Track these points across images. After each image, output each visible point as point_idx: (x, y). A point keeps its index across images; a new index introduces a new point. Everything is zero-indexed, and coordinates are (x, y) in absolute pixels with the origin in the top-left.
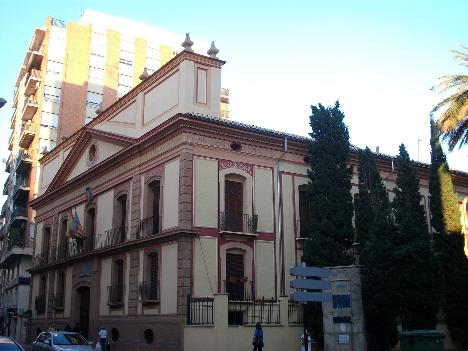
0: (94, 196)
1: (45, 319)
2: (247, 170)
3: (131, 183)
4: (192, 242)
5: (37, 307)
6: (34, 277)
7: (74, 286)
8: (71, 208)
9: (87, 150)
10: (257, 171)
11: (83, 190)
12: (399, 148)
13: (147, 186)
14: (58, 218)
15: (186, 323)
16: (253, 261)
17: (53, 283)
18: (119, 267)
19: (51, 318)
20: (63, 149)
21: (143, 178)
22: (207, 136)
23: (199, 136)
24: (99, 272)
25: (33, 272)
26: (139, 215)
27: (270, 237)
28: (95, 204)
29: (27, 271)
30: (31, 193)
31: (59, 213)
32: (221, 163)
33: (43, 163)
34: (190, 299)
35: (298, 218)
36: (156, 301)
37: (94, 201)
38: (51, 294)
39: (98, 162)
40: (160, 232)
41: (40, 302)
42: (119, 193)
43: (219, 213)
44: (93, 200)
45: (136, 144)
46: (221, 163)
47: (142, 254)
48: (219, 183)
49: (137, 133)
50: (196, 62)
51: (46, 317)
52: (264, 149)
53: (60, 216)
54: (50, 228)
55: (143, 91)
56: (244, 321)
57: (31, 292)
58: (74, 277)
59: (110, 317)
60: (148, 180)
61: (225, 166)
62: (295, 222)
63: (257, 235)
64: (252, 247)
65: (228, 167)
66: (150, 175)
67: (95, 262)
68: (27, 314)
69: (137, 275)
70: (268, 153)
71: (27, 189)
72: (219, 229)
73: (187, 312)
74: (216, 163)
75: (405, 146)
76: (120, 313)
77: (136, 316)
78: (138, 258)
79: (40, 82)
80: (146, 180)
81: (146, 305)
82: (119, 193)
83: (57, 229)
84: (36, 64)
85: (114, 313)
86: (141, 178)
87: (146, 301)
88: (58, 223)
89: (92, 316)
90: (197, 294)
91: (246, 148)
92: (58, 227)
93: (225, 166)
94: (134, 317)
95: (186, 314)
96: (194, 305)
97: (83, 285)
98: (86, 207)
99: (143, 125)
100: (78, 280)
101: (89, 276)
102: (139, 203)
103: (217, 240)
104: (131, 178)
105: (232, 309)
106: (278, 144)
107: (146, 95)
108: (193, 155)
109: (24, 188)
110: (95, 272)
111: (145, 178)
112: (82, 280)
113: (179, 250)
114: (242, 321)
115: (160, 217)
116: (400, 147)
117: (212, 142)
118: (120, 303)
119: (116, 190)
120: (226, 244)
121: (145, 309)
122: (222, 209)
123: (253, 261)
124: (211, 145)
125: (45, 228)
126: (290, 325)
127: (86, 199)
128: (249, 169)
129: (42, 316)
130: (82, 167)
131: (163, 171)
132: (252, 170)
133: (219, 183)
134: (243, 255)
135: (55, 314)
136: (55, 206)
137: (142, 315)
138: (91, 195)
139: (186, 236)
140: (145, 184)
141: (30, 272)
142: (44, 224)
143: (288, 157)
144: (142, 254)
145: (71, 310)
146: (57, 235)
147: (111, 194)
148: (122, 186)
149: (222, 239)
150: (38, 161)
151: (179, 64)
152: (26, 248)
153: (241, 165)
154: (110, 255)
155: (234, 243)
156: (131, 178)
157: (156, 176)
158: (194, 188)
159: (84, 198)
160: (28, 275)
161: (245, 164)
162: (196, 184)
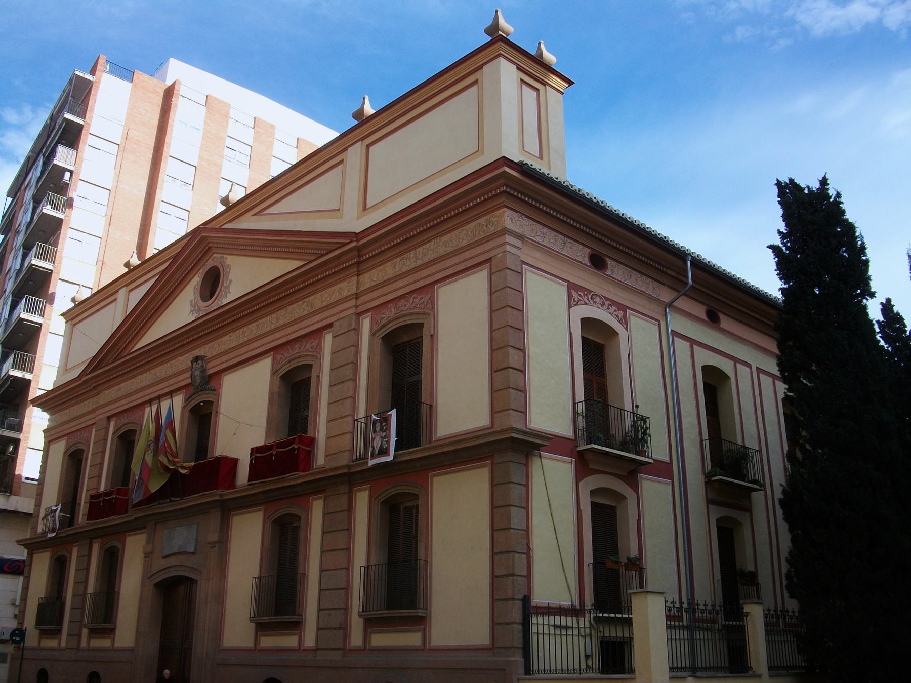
0: (211, 376)
1: (59, 649)
2: (617, 316)
3: (328, 338)
4: (527, 465)
5: (41, 620)
6: (35, 556)
7: (147, 575)
8: (142, 405)
9: (196, 280)
10: (634, 321)
11: (183, 361)
12: (880, 307)
13: (378, 342)
14: (107, 428)
15: (522, 671)
16: (639, 521)
17: (87, 569)
18: (59, 568)
19: (78, 648)
20: (127, 285)
21: (366, 323)
22: (547, 226)
23: (532, 222)
24: (223, 544)
25: (33, 546)
26: (354, 407)
27: (662, 470)
28: (216, 391)
29: (19, 542)
30: (33, 385)
31: (109, 418)
32: (573, 291)
33: (72, 319)
34: (528, 609)
35: (706, 436)
36: (294, 618)
37: (212, 385)
38: (80, 595)
39: (225, 301)
40: (424, 442)
41: (50, 614)
42: (290, 362)
43: (574, 403)
44: (208, 382)
45: (354, 244)
46: (573, 291)
47: (362, 499)
48: (571, 334)
49: (353, 222)
50: (519, 68)
51: (63, 644)
52: (644, 277)
53: (112, 424)
54: (82, 451)
55: (363, 139)
56: (536, 668)
57: (26, 589)
58: (148, 555)
59: (256, 649)
60: (383, 326)
61: (579, 300)
62: (702, 441)
63: (652, 461)
64: (635, 487)
65: (586, 304)
66: (389, 313)
67: (214, 519)
68: (16, 635)
69: (348, 550)
70: (650, 287)
71: (28, 376)
72: (575, 441)
73: (521, 641)
74: (563, 290)
75: (892, 303)
76: (53, 643)
77: (346, 650)
78: (350, 509)
79: (72, 172)
80: (376, 328)
81: (95, 632)
82: (290, 362)
83: (104, 452)
84: (71, 136)
85: (268, 641)
86: (358, 323)
87: (266, 619)
88: (106, 440)
89: (201, 645)
90: (540, 598)
91: (615, 270)
92: (105, 448)
93: (579, 300)
94: (341, 652)
95: (521, 646)
96: (538, 623)
97: (174, 574)
98: (187, 400)
99: (365, 208)
100: (161, 563)
101: (193, 553)
102: (355, 379)
103: (573, 465)
104: (330, 325)
105: (607, 634)
106: (669, 272)
107: (371, 149)
108: (523, 262)
109: (18, 374)
110: (215, 543)
111: (116, 424)
112: (172, 561)
113: (493, 485)
114: (624, 665)
115: (424, 408)
116: (882, 303)
117: (555, 240)
118: (109, 626)
119: (278, 357)
120: (590, 478)
121: (372, 633)
122: (580, 396)
123: (639, 521)
124: (555, 248)
125: (72, 450)
126: (674, 674)
127: (189, 381)
128: (621, 314)
129: (52, 643)
130: (181, 312)
131: (432, 302)
132: (625, 316)
133: (571, 334)
134: (613, 509)
135: (89, 639)
136: (101, 402)
137: (366, 648)
138: (203, 371)
139: (507, 449)
140: (114, 434)
141: (25, 546)
142: (67, 444)
143: (683, 303)
144: (362, 499)
145: (138, 632)
146: (102, 464)
147: (265, 366)
148: (297, 346)
149: (584, 465)
150: (62, 315)
151: (481, 67)
152: (12, 496)
153: (607, 303)
154: (256, 505)
155: (602, 475)
156: (330, 325)
157: (411, 314)
158: (513, 343)
159: (185, 379)
160: (20, 554)
161: (613, 303)
162: (530, 330)
